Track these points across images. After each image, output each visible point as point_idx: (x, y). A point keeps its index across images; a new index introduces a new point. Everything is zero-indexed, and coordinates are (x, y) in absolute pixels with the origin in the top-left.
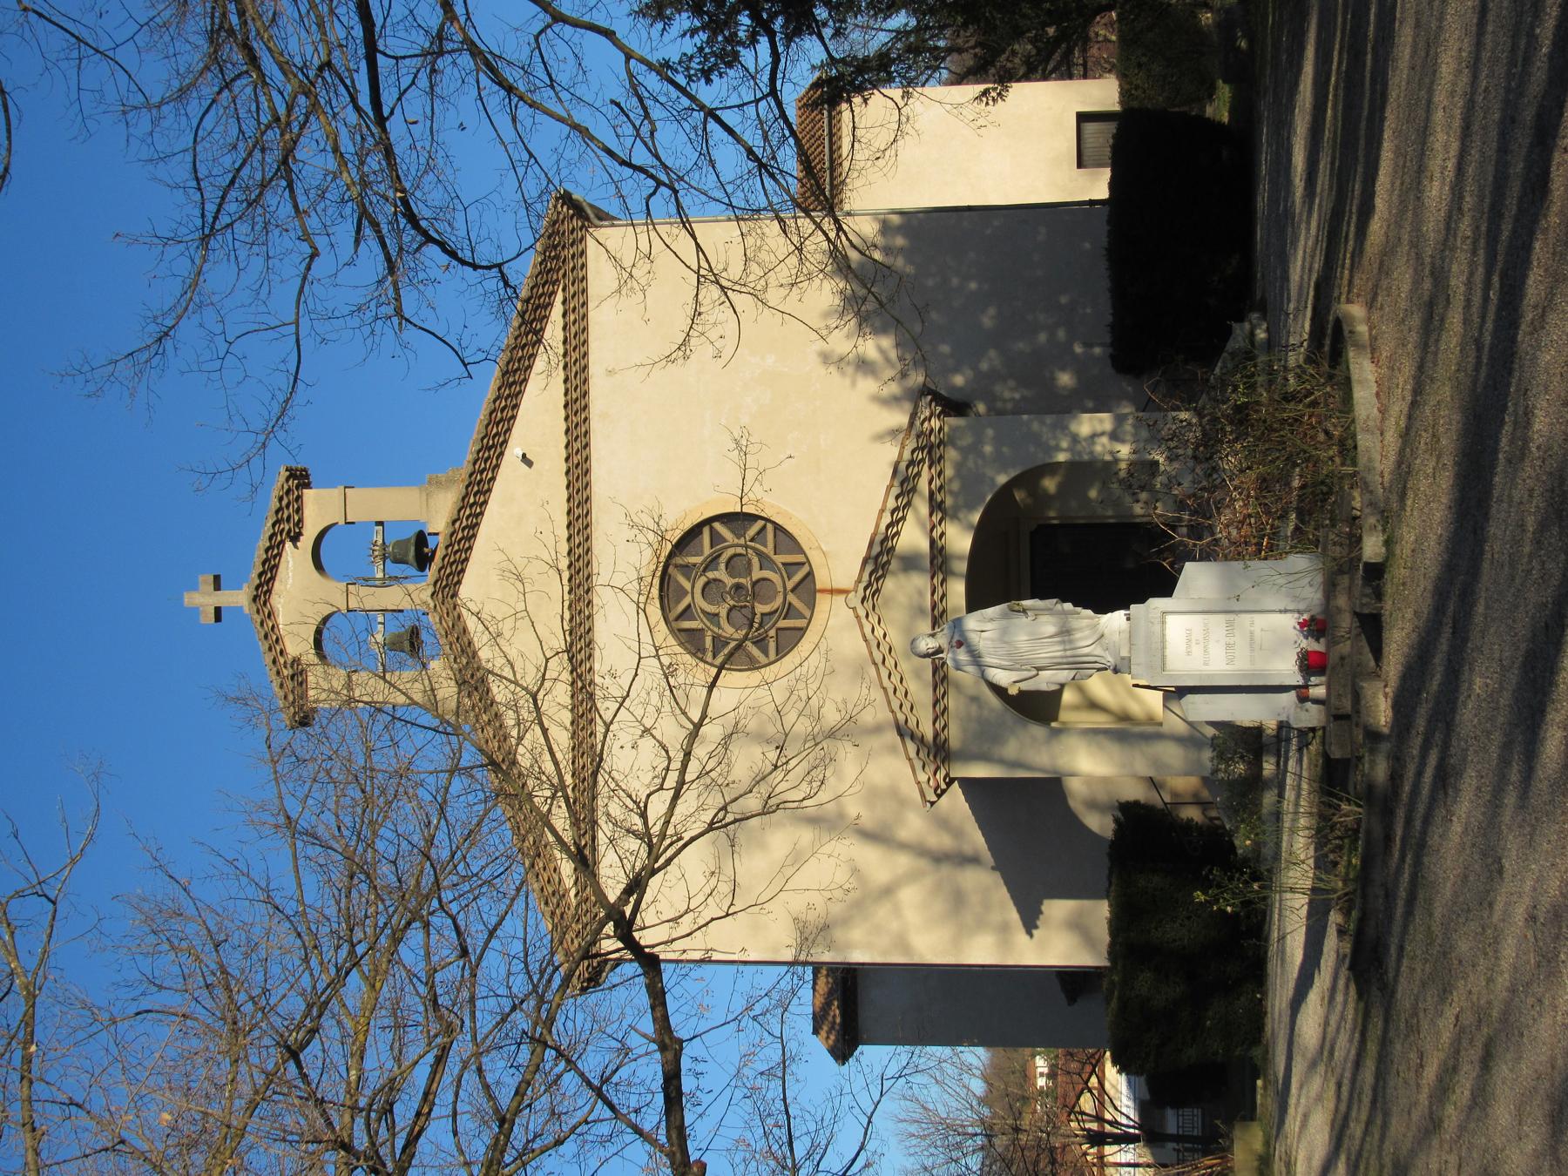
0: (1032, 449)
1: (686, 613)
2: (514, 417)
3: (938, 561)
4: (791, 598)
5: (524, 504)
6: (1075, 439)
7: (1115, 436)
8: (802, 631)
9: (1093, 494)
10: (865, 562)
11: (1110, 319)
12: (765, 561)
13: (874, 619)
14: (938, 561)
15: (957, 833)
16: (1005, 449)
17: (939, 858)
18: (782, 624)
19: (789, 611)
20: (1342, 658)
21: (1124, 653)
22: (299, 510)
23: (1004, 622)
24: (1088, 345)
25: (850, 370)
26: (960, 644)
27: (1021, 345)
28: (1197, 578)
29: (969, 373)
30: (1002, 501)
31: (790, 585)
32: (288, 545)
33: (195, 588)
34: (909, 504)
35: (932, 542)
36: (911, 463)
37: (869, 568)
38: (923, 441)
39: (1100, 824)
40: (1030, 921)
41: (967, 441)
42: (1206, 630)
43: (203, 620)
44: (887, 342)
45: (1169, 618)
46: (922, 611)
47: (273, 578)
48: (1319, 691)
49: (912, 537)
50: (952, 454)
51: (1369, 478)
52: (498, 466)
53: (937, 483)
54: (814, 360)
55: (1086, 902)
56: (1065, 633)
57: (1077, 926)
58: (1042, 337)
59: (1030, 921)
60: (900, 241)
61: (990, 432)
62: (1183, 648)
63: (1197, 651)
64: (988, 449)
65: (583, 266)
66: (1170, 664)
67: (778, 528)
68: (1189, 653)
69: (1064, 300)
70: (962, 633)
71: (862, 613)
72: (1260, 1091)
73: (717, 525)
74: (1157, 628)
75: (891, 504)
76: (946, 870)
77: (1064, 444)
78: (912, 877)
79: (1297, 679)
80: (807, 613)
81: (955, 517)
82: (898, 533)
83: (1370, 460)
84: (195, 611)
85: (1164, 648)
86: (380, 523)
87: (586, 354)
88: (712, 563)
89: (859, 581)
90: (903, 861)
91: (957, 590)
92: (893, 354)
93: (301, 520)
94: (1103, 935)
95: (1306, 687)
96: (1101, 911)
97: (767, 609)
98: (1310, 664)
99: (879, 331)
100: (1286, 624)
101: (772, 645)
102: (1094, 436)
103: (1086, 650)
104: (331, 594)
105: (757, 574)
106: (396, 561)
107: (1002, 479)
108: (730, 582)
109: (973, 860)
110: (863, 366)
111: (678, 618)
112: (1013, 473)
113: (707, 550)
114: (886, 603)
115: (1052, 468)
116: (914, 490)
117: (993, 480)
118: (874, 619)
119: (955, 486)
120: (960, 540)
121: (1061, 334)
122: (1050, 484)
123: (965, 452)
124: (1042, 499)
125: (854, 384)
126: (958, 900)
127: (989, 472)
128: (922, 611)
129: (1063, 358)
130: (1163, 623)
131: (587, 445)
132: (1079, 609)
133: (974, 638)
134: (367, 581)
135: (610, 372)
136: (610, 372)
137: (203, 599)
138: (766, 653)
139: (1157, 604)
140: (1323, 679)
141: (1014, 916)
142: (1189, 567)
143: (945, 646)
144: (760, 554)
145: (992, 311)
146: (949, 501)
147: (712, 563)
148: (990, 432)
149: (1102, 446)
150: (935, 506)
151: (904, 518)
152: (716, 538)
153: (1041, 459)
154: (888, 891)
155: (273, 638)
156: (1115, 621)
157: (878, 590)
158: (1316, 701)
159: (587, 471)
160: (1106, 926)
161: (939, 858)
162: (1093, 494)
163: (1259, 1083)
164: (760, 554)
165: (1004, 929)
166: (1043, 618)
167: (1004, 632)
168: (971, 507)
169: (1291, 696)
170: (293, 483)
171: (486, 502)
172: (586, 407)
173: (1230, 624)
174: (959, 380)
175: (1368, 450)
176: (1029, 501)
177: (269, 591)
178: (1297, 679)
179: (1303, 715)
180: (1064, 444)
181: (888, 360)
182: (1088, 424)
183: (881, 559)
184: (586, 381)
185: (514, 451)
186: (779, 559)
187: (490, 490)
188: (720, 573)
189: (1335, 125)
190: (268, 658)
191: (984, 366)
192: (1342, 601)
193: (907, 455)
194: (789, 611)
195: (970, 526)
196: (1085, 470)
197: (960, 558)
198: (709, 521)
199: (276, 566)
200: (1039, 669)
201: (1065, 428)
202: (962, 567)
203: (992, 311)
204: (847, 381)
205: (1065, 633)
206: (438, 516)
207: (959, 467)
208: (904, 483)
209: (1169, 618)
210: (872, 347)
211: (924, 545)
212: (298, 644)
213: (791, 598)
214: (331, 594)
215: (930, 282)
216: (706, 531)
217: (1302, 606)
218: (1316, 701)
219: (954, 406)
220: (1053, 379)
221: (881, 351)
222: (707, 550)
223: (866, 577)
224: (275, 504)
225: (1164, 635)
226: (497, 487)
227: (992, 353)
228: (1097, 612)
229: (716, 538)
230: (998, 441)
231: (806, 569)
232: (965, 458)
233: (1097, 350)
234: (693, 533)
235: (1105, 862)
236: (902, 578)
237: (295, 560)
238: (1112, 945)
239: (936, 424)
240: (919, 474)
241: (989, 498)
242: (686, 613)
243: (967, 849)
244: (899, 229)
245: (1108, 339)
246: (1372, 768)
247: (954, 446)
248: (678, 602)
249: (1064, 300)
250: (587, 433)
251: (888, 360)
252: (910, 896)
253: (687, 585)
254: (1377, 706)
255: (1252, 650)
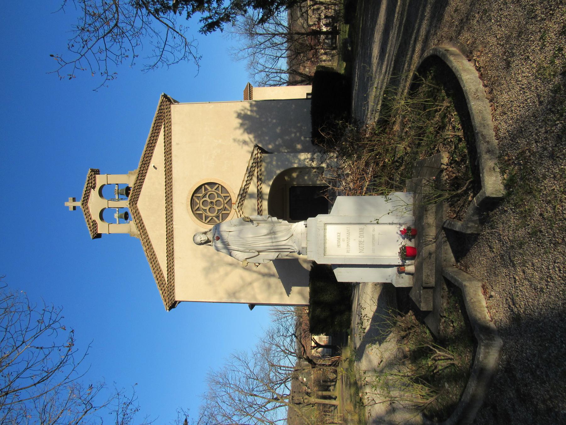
0: (287, 163)
1: (198, 209)
2: (152, 156)
3: (260, 195)
4: (225, 205)
5: (154, 179)
6: (300, 160)
7: (312, 160)
8: (229, 214)
9: (306, 178)
10: (238, 195)
11: (311, 130)
12: (219, 195)
13: (241, 212)
14: (260, 195)
15: (269, 268)
16: (279, 163)
17: (264, 275)
18: (223, 212)
19: (225, 209)
20: (430, 254)
21: (304, 245)
22: (95, 180)
23: (241, 227)
24: (305, 137)
25: (241, 143)
26: (218, 238)
27: (287, 137)
28: (343, 204)
29: (273, 145)
30: (280, 177)
31: (225, 202)
32: (92, 190)
33: (68, 201)
34: (251, 179)
35: (258, 190)
36: (252, 167)
37: (240, 197)
38: (256, 161)
39: (307, 267)
40: (288, 292)
41: (268, 160)
42: (348, 233)
43: (70, 210)
44: (251, 136)
45: (328, 227)
46: (255, 210)
47: (88, 199)
48: (411, 268)
49: (252, 188)
50: (264, 164)
51: (485, 132)
52: (147, 169)
53: (259, 173)
54: (232, 141)
55: (303, 288)
56: (272, 233)
57: (301, 293)
58: (293, 135)
59: (288, 292)
60: (255, 109)
61: (275, 158)
62: (335, 242)
63: (343, 245)
64: (274, 163)
65: (170, 115)
66: (328, 252)
67: (222, 186)
68: (338, 246)
69: (299, 125)
70: (219, 232)
71: (238, 211)
72: (349, 340)
73: (206, 186)
74: (322, 232)
75: (246, 179)
76: (266, 278)
77: (296, 162)
78: (257, 280)
79: (399, 262)
80: (230, 209)
81: (264, 183)
82: (248, 187)
83: (484, 119)
84: (68, 207)
85: (325, 243)
86: (117, 184)
87: (171, 139)
88: (204, 196)
89: (237, 201)
90: (255, 276)
91: (265, 204)
92: (253, 140)
93: (95, 183)
94: (308, 296)
95: (403, 265)
96: (308, 289)
97: (219, 208)
98: (406, 254)
99: (249, 133)
100: (394, 231)
101: (208, 220)
102: (305, 159)
103: (284, 243)
104: (103, 203)
105: (216, 199)
106: (121, 194)
107: (278, 172)
108: (209, 201)
109: (273, 275)
110: (245, 142)
111: (196, 210)
112: (282, 170)
113: (203, 192)
114: (245, 207)
115: (294, 170)
116: (253, 175)
117: (275, 172)
118: (241, 212)
119: (265, 174)
120: (266, 190)
121: (298, 134)
122: (294, 175)
123: (268, 163)
124: (292, 179)
125: (242, 148)
126: (269, 286)
127: (274, 169)
128: (255, 210)
129: (298, 141)
130: (325, 229)
131: (171, 164)
132: (280, 220)
133: (225, 235)
134: (113, 199)
135: (177, 144)
136: (177, 144)
137: (70, 204)
138: (219, 220)
139: (321, 218)
140: (413, 261)
141: (284, 290)
142: (339, 198)
143: (211, 239)
144: (217, 193)
145: (279, 128)
146: (263, 178)
147: (204, 196)
148: (275, 158)
149: (308, 163)
150: (259, 179)
151: (250, 183)
152: (206, 189)
153: (290, 166)
154: (250, 284)
155: (88, 215)
156: (299, 226)
157: (242, 204)
158: (408, 274)
159: (171, 171)
160: (308, 294)
161: (264, 275)
162: (306, 178)
163: (349, 337)
164: (217, 193)
165: (281, 294)
166: (262, 225)
167: (240, 231)
168: (270, 180)
169: (395, 269)
170: (93, 173)
171: (144, 179)
172: (171, 153)
173: (362, 230)
174: (270, 147)
175: (480, 112)
176: (289, 179)
177: (87, 202)
178: (399, 262)
179: (401, 281)
180: (296, 162)
181: (251, 141)
182: (303, 156)
183: (243, 194)
184: (171, 146)
185: (152, 165)
186: (222, 195)
187: (145, 176)
188: (207, 198)
189: (402, 14)
190: (86, 220)
191: (277, 143)
192: (430, 219)
193: (251, 165)
194: (225, 209)
195: (269, 185)
196: (304, 170)
197: (266, 194)
198: (204, 185)
199: (89, 195)
200: (259, 252)
201: (297, 157)
202: (267, 197)
203: (279, 128)
204: (240, 147)
205: (272, 233)
206: (130, 180)
207: (266, 168)
208: (250, 173)
209: (328, 227)
210: (247, 137)
211: (255, 191)
212: (95, 216)
213: (225, 205)
214: (103, 203)
215: (263, 120)
216: (203, 187)
217: (401, 221)
218: (408, 274)
219: (263, 151)
220: (296, 146)
221: (250, 139)
222: (203, 192)
223: (239, 200)
224: (88, 179)
225: (325, 236)
226: (148, 175)
227: (279, 139)
228: (289, 222)
229: (206, 189)
230: (277, 161)
231: (229, 198)
232: (268, 165)
233: (308, 139)
234: (200, 188)
235: (308, 277)
236: (249, 200)
237: (94, 194)
238: (310, 299)
239: (259, 155)
240: (254, 170)
241: (275, 177)
242: (198, 209)
243: (272, 273)
244: (255, 105)
245: (311, 136)
246: (485, 357)
247: (265, 162)
248: (196, 206)
249: (299, 125)
250: (171, 160)
251: (251, 141)
252: (256, 285)
253: (198, 202)
254: (479, 301)
255: (373, 245)
